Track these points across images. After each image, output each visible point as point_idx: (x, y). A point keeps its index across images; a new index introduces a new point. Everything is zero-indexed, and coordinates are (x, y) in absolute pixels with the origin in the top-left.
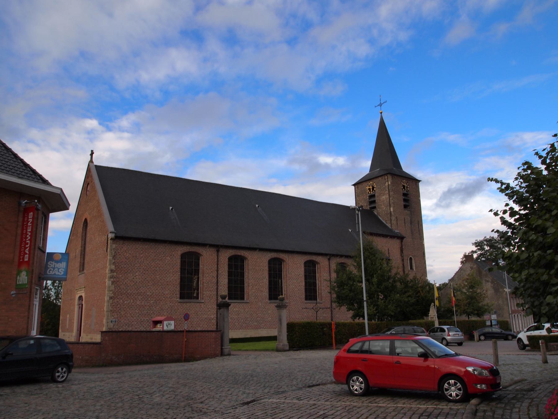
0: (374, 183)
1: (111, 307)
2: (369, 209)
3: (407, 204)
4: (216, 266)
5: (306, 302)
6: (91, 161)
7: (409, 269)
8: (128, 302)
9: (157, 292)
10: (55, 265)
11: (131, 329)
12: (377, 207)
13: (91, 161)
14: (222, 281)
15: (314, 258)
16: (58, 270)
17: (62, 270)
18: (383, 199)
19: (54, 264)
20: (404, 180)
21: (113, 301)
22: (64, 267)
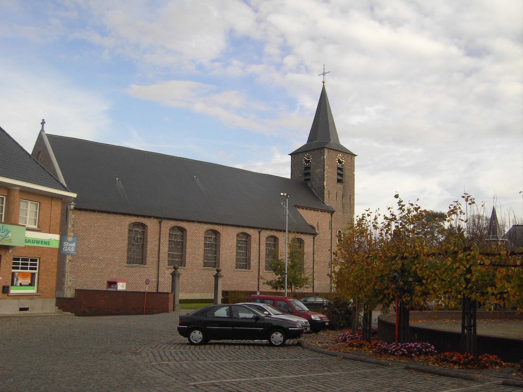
0: (310, 155)
1: (70, 268)
2: (303, 181)
3: (341, 178)
4: (158, 235)
5: (236, 270)
6: (42, 130)
7: (337, 242)
8: (84, 265)
9: (108, 257)
10: (68, 245)
11: (86, 287)
12: (311, 179)
13: (42, 130)
14: (163, 250)
15: (246, 231)
16: (71, 248)
17: (73, 248)
18: (318, 172)
19: (68, 244)
20: (339, 154)
21: (72, 263)
22: (74, 246)
